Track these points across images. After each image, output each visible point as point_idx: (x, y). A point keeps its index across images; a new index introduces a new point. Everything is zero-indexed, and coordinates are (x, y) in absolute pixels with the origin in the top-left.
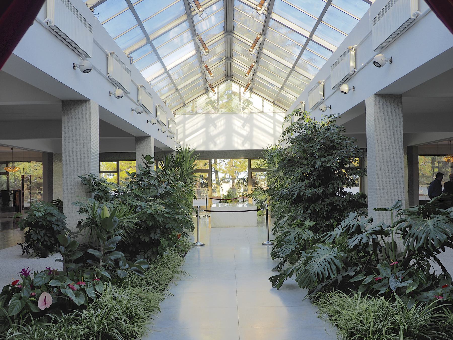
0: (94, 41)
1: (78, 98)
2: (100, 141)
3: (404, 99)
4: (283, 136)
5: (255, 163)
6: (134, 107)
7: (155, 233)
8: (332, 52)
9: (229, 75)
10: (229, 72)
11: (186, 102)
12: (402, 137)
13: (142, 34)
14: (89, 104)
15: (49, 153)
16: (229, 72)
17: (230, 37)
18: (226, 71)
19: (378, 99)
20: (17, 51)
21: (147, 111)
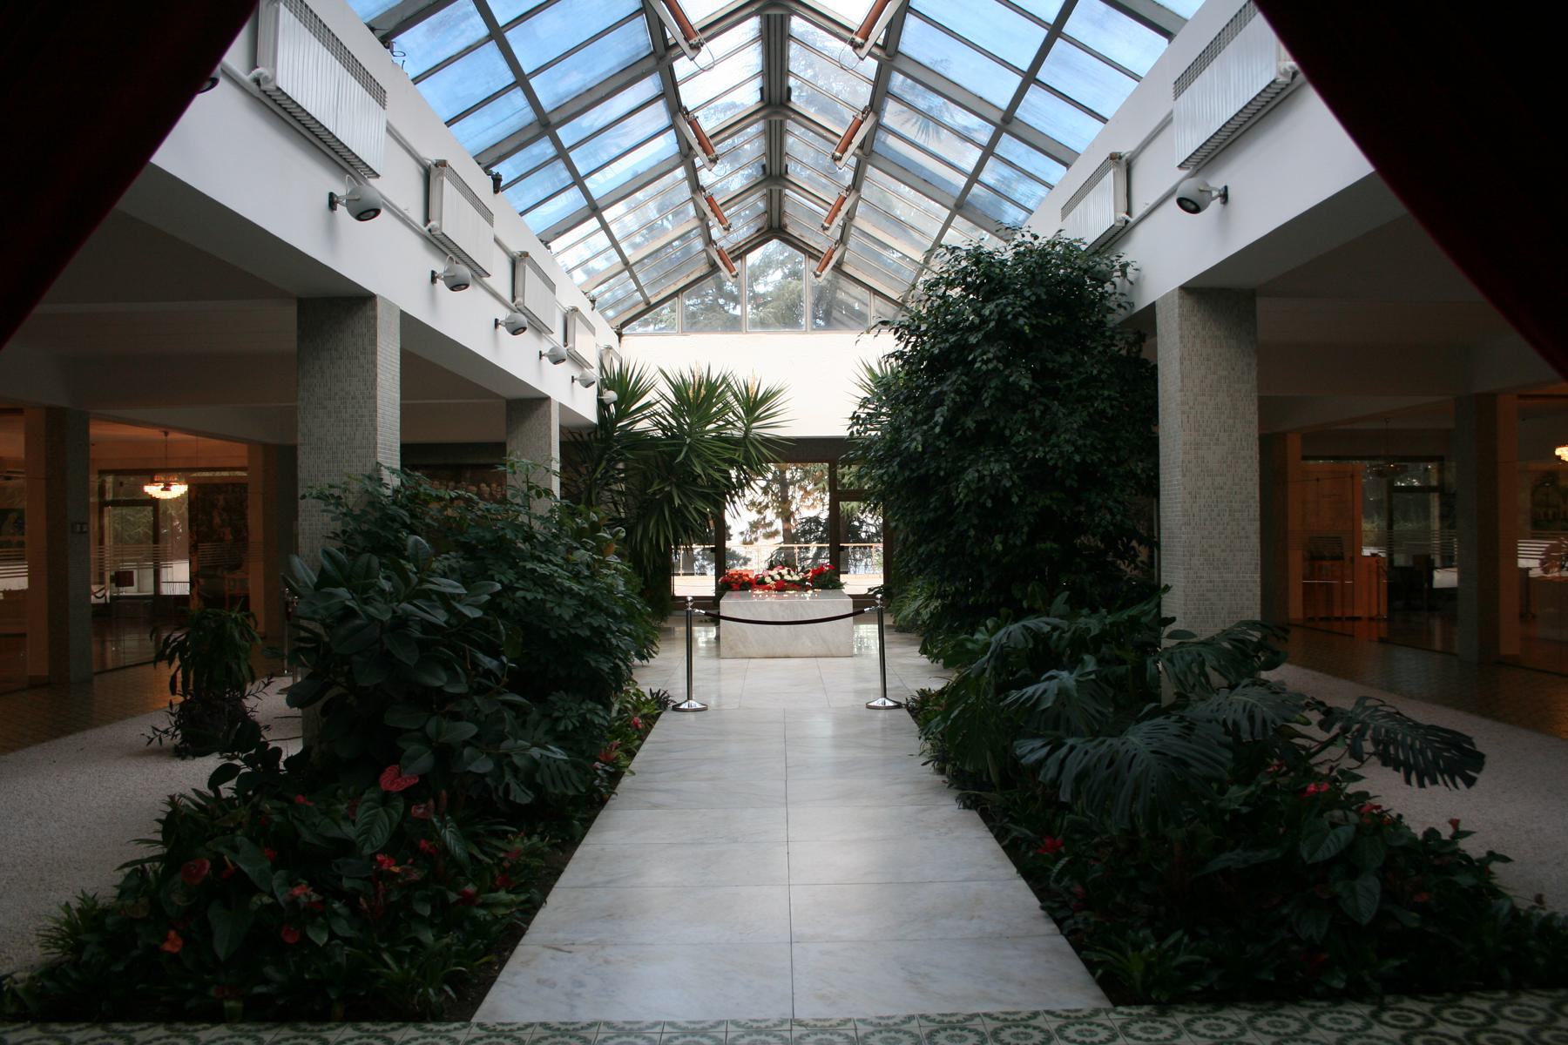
0: (390, 131)
1: (535, 395)
2: (403, 408)
3: (1262, 304)
4: (771, 567)
5: (848, 474)
6: (503, 314)
7: (155, 872)
8: (1104, 120)
9: (775, 224)
10: (775, 215)
11: (653, 301)
12: (1254, 408)
13: (529, 109)
14: (374, 308)
15: (51, 410)
16: (775, 215)
17: (778, 118)
18: (768, 211)
19: (1189, 302)
20: (166, 157)
21: (540, 329)
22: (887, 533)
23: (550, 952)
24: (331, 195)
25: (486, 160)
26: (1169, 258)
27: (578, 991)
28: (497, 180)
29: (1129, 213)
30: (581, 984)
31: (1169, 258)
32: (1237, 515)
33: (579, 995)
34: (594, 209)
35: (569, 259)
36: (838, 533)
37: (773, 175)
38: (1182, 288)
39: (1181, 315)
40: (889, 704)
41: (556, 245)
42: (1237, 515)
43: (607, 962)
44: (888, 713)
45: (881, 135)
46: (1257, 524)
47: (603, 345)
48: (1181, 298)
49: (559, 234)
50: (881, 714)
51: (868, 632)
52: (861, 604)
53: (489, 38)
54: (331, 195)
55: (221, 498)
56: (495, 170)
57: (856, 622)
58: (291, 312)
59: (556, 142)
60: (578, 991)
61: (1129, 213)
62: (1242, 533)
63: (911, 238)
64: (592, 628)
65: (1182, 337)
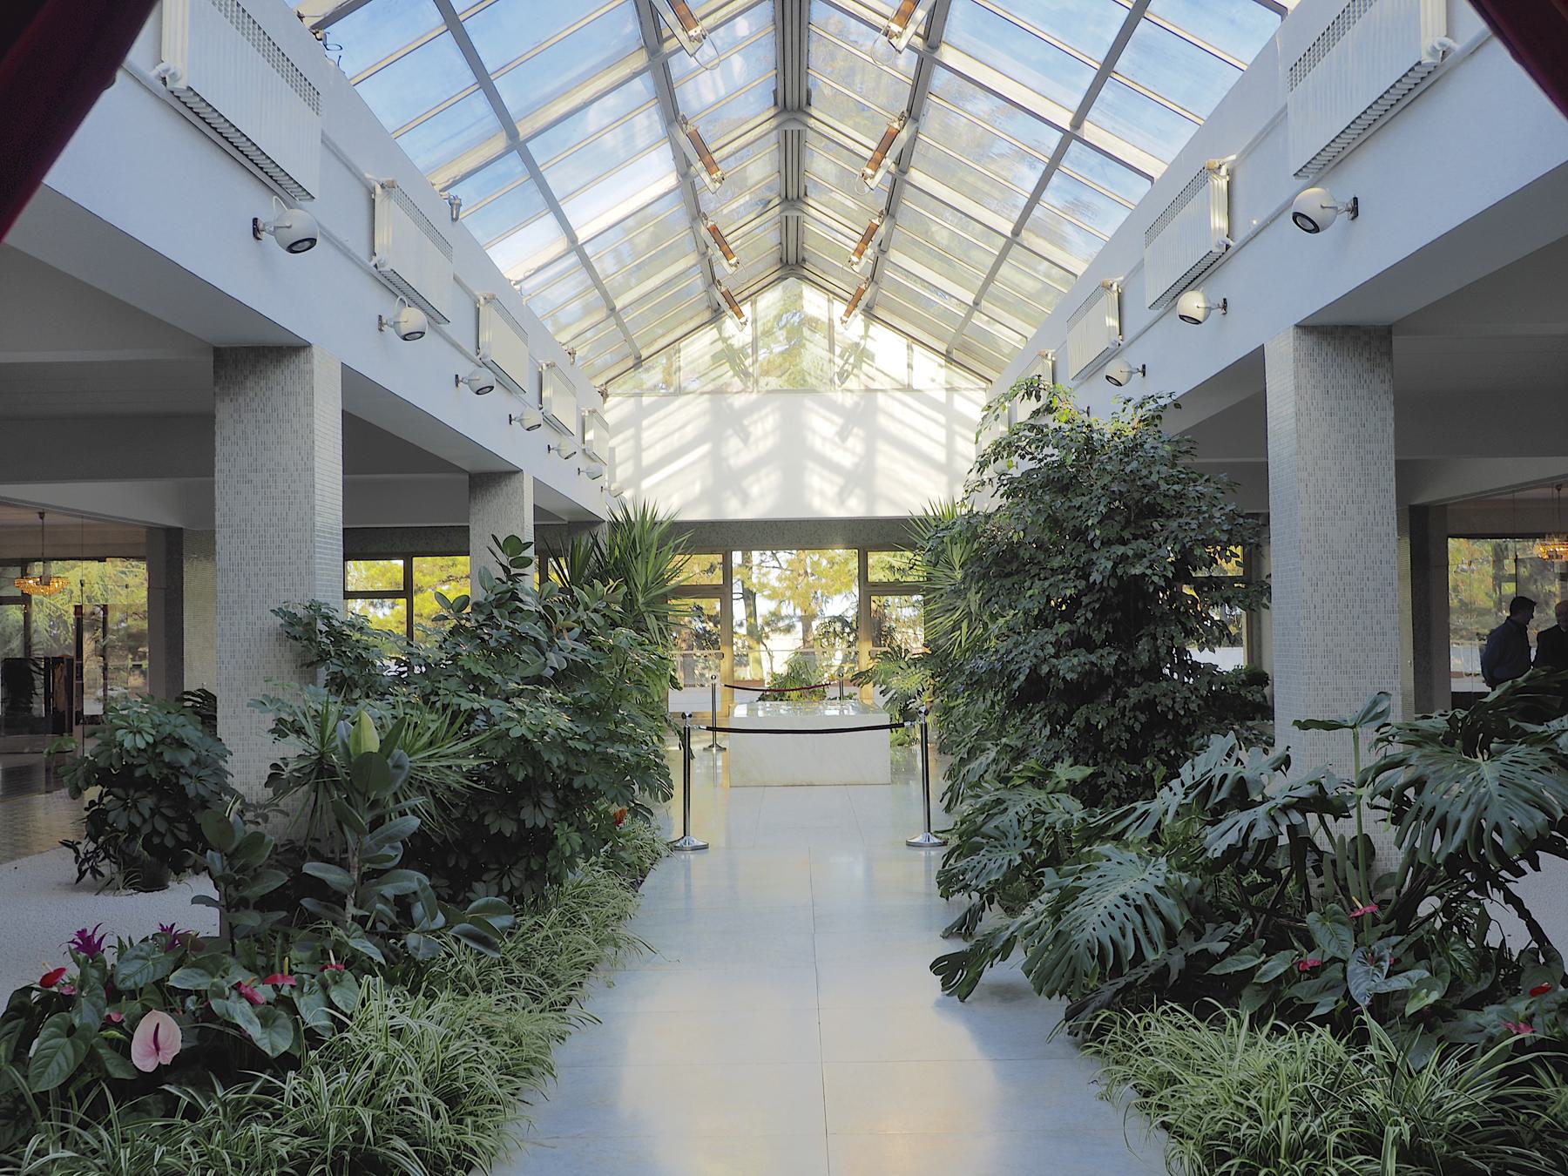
0: (325, 141)
2: (347, 487)
3: (1398, 341)
4: (981, 470)
5: (882, 565)
6: (465, 369)
7: (538, 804)
8: (1151, 178)
9: (792, 259)
10: (792, 248)
11: (645, 354)
12: (1392, 473)
13: (493, 116)
14: (309, 361)
16: (792, 248)
17: (795, 127)
18: (783, 245)
19: (1309, 341)
20: (59, 177)
21: (508, 384)
53: (508, 151)
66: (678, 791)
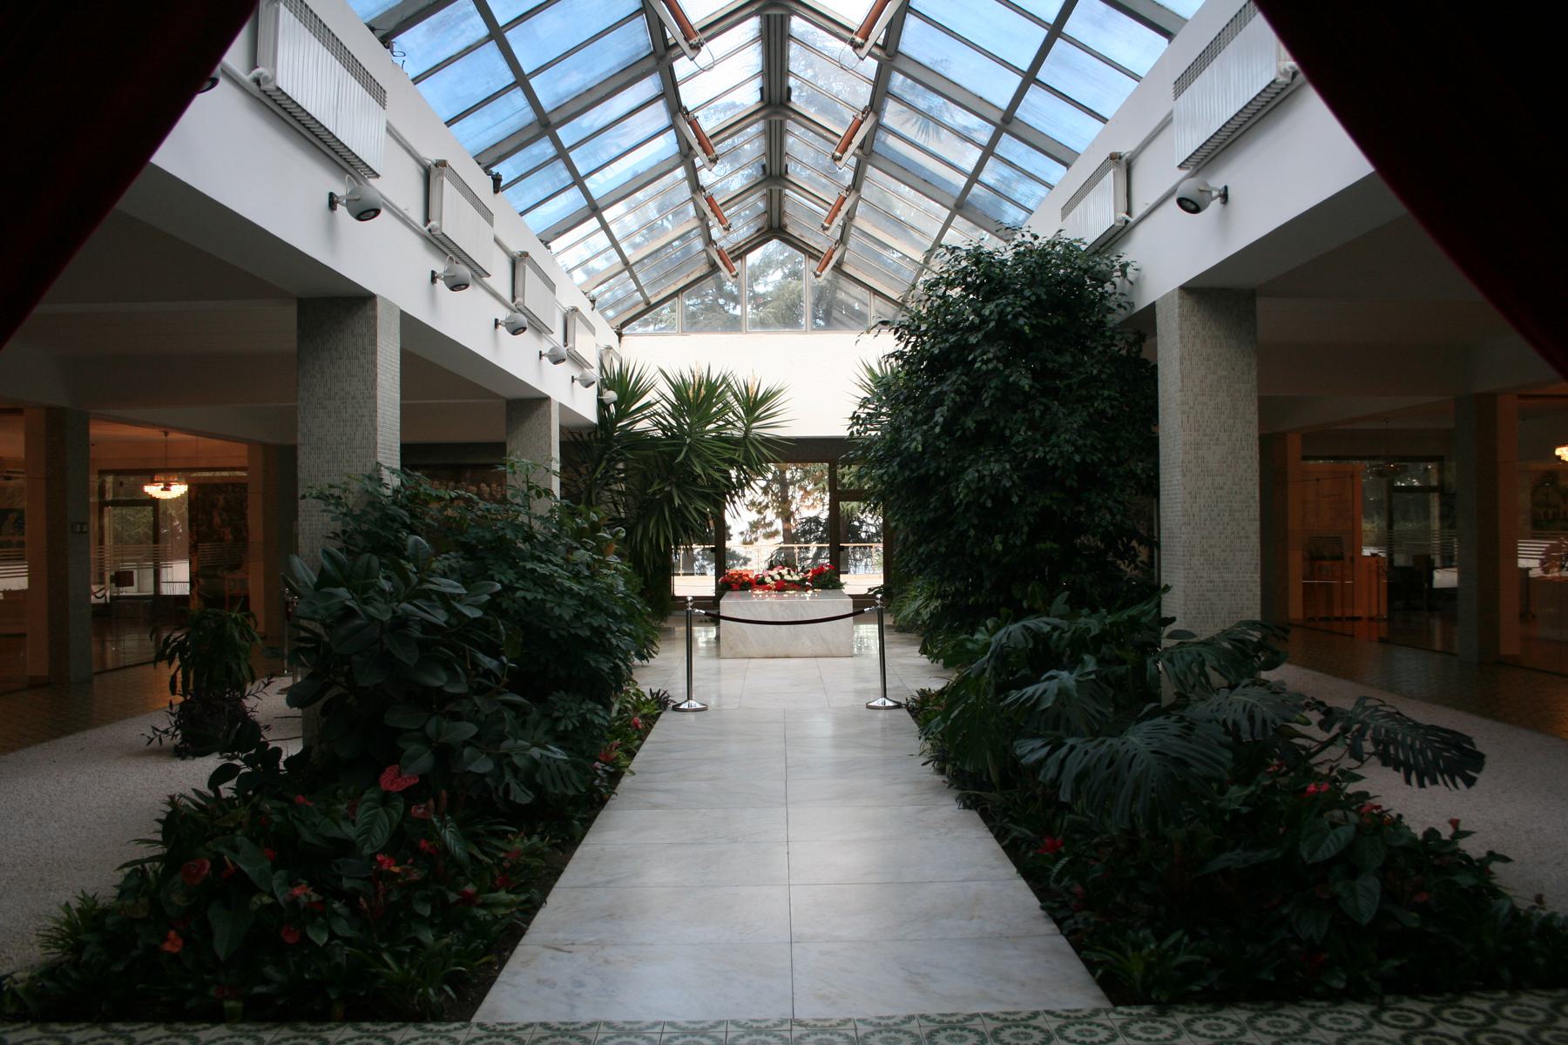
0: (390, 131)
1: (535, 395)
2: (403, 408)
3: (1262, 304)
4: (771, 567)
5: (848, 474)
6: (503, 314)
8: (1104, 120)
9: (775, 224)
10: (775, 215)
11: (653, 301)
12: (1254, 408)
13: (529, 109)
14: (374, 308)
15: (51, 410)
16: (775, 215)
17: (778, 118)
18: (768, 211)
19: (1189, 302)
20: (166, 157)
21: (540, 329)
22: (887, 533)
23: (550, 952)
24: (331, 195)
25: (486, 160)
26: (1169, 258)
27: (578, 991)
28: (497, 180)
29: (1129, 213)
30: (581, 984)
31: (1169, 258)
32: (1237, 515)
33: (579, 995)
34: (594, 209)
35: (569, 259)
36: (838, 533)
37: (773, 175)
38: (1182, 288)
39: (1181, 315)
40: (889, 704)
41: (556, 245)
42: (1237, 515)
43: (607, 962)
44: (888, 713)
45: (881, 135)
46: (1257, 524)
47: (603, 345)
48: (1181, 298)
49: (559, 234)
50: (881, 714)
51: (868, 632)
52: (861, 604)
54: (331, 195)
55: (221, 498)
56: (495, 170)
57: (856, 622)
58: (291, 312)
59: (556, 142)
60: (578, 991)
61: (1129, 213)
62: (1242, 533)
63: (911, 238)
64: (592, 628)
65: (1182, 337)
66: (1509, 1037)
